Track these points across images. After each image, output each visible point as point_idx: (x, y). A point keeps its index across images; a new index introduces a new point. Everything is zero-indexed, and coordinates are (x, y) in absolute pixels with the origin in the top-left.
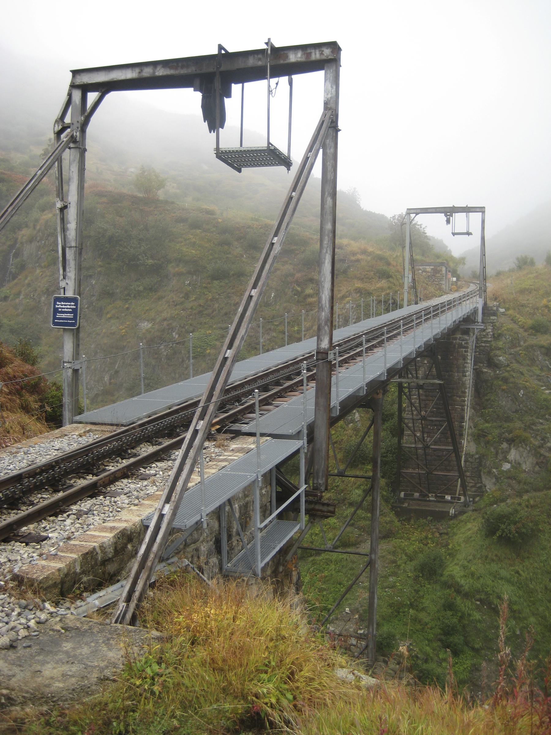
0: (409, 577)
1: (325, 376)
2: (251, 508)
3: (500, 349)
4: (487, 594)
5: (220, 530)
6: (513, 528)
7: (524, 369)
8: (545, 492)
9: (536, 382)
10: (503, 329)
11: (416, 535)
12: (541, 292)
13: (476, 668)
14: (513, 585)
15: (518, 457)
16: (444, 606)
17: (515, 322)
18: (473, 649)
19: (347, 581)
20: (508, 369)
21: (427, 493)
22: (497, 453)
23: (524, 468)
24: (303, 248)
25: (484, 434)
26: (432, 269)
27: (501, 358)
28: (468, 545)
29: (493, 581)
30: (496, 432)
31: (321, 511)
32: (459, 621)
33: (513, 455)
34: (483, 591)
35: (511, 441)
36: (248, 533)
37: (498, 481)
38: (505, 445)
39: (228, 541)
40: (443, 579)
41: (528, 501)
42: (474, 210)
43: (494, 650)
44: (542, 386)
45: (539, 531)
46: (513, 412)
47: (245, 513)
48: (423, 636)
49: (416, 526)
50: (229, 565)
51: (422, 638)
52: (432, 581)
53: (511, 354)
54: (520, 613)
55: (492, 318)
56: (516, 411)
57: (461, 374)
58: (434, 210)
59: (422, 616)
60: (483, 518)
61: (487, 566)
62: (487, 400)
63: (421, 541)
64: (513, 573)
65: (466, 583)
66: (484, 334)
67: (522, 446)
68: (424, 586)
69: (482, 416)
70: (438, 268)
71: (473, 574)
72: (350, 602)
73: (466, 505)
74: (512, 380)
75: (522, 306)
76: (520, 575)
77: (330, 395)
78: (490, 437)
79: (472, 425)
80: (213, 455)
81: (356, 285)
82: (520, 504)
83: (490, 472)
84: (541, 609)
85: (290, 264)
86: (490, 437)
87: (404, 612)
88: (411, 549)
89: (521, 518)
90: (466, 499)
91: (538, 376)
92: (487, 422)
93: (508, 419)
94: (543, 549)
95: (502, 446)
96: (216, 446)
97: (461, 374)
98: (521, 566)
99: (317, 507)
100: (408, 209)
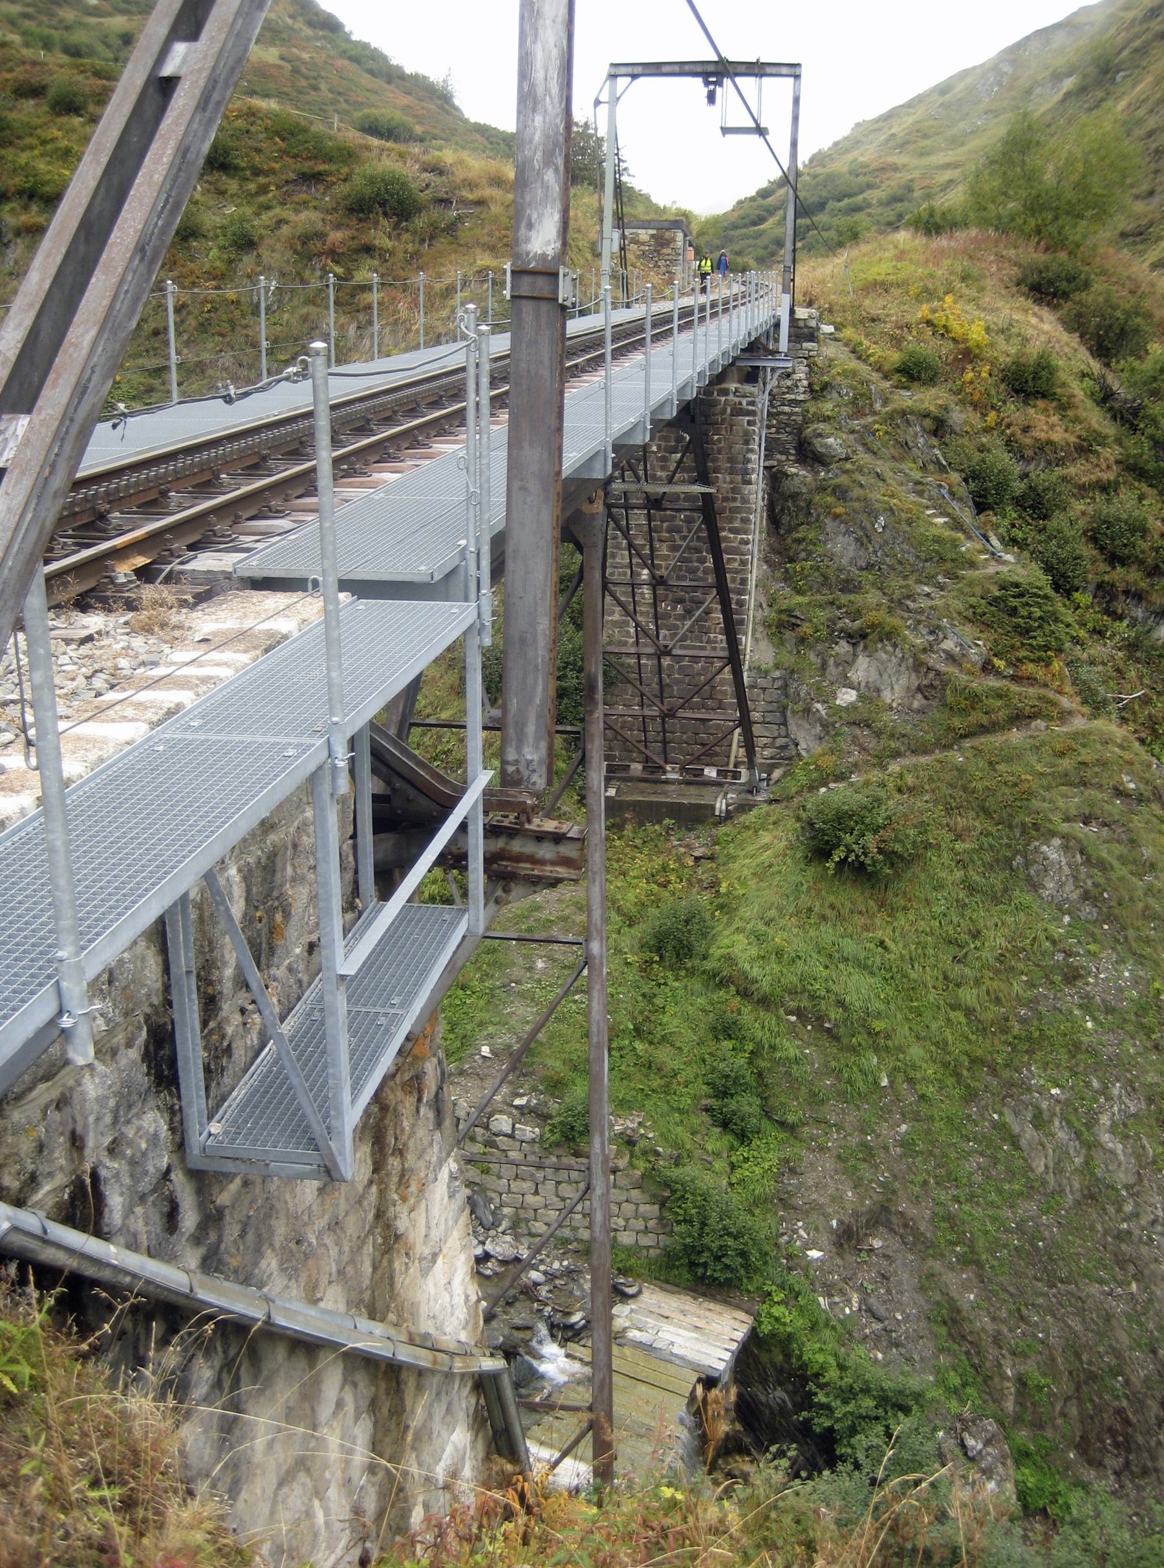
0: (628, 964)
1: (546, 362)
2: (289, 871)
3: (827, 419)
4: (813, 997)
5: (167, 988)
6: (870, 840)
7: (883, 467)
8: (938, 754)
9: (913, 497)
10: (834, 372)
11: (642, 863)
12: (914, 290)
13: (790, 1168)
14: (872, 973)
15: (873, 676)
16: (714, 1029)
17: (859, 358)
18: (782, 1124)
19: (482, 980)
20: (848, 466)
21: (661, 762)
22: (824, 666)
23: (888, 701)
24: (345, 170)
25: (793, 620)
26: (652, 236)
27: (831, 440)
28: (764, 885)
29: (826, 967)
30: (822, 615)
31: (533, 860)
32: (750, 1063)
33: (863, 669)
34: (804, 990)
35: (858, 638)
36: (280, 972)
37: (828, 733)
38: (843, 647)
39: (205, 1024)
40: (708, 965)
41: (901, 776)
42: (773, 70)
43: (831, 1126)
44: (927, 508)
45: (928, 846)
46: (861, 569)
47: (268, 895)
48: (668, 1102)
49: (638, 842)
50: (215, 1128)
51: (666, 1107)
52: (683, 973)
53: (852, 432)
54: (888, 1037)
55: (805, 345)
56: (869, 567)
57: (739, 478)
58: (677, 69)
59: (663, 1054)
60: (798, 819)
61: (812, 933)
62: (799, 541)
63: (651, 877)
64: (872, 946)
65: (763, 975)
66: (789, 383)
67: (883, 649)
68: (665, 984)
69: (787, 578)
70: (667, 235)
71: (779, 953)
72: (491, 1029)
73: (752, 789)
74: (856, 492)
75: (873, 320)
76: (886, 949)
77: (561, 436)
78: (807, 628)
79: (763, 600)
80: (123, 663)
81: (479, 262)
82: (883, 785)
83: (807, 711)
84: (934, 1026)
85: (315, 208)
86: (807, 628)
87: (621, 1049)
88: (631, 896)
89: (889, 818)
90: (752, 775)
91: (917, 483)
92: (799, 592)
93: (849, 586)
94: (939, 887)
95: (837, 648)
96: (132, 629)
97: (739, 478)
98: (889, 931)
99: (517, 846)
100: (613, 65)
